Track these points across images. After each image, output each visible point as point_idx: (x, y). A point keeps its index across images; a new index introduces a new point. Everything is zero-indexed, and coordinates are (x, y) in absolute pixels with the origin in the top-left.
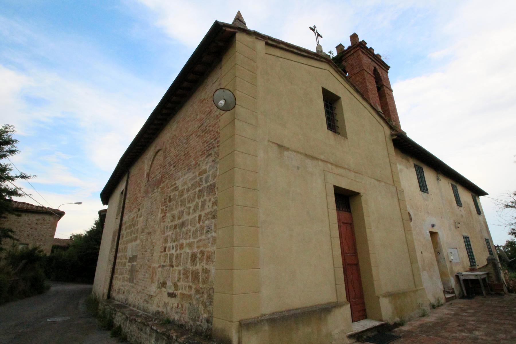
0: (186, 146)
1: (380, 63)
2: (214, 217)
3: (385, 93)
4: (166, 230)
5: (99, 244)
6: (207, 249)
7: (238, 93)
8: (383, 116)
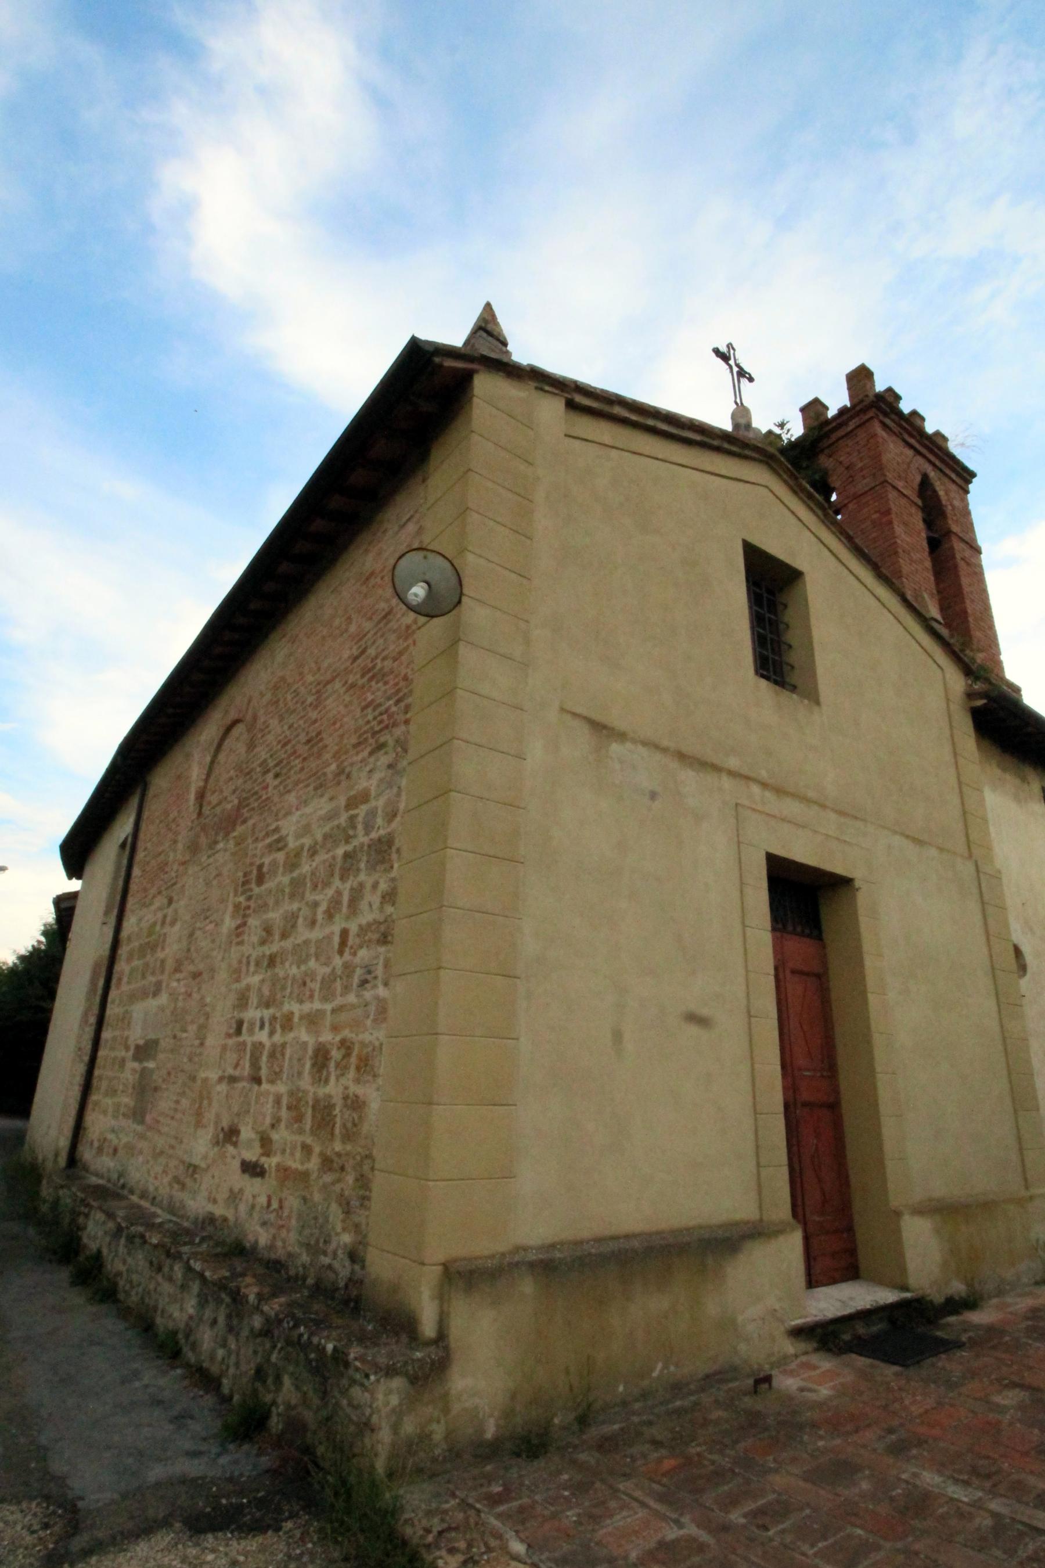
0: (314, 715)
1: (943, 461)
2: (385, 939)
3: (954, 557)
4: (244, 969)
5: (51, 994)
6: (361, 1037)
7: (471, 563)
8: (944, 632)
